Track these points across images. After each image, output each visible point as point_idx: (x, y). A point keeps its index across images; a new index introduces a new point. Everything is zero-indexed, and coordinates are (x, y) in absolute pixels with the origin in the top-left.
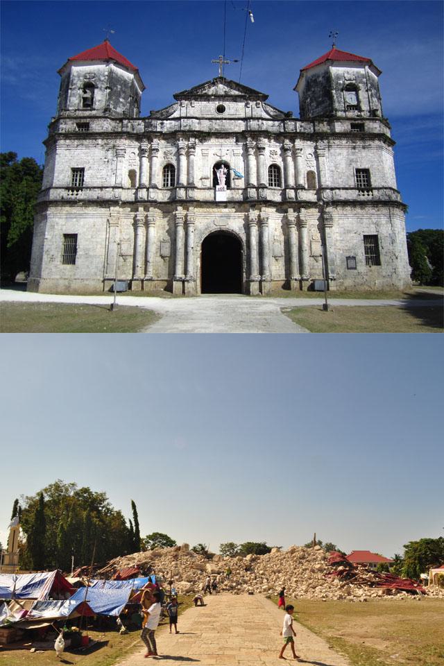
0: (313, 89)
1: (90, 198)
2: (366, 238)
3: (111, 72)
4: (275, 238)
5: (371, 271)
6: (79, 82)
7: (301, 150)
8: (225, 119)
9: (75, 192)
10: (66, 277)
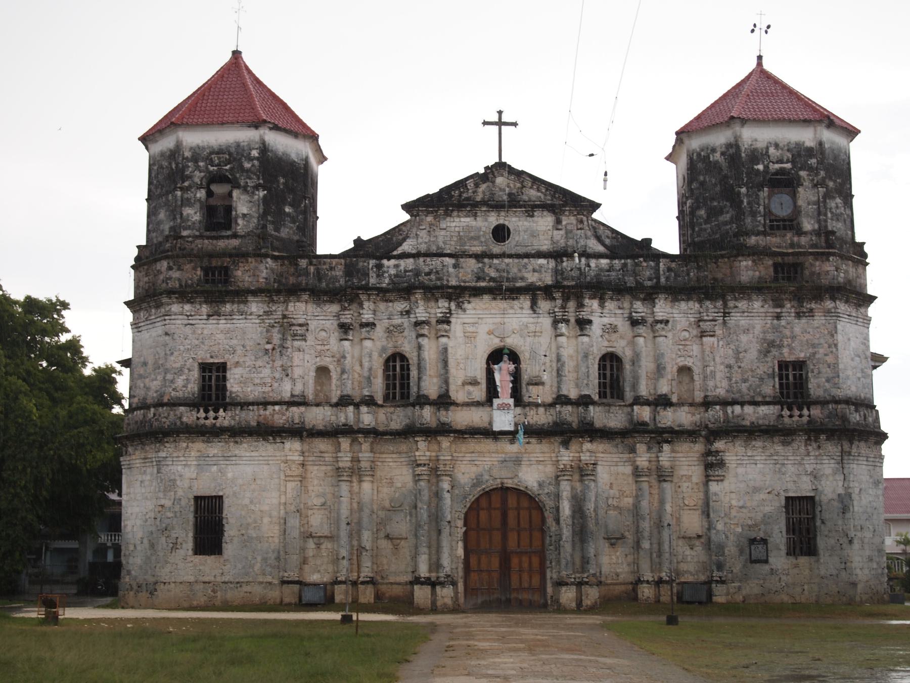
0: (701, 178)
1: (243, 424)
2: (791, 502)
3: (264, 149)
4: (610, 501)
5: (796, 566)
6: (197, 173)
7: (667, 322)
8: (510, 256)
9: (211, 414)
10: (206, 579)
